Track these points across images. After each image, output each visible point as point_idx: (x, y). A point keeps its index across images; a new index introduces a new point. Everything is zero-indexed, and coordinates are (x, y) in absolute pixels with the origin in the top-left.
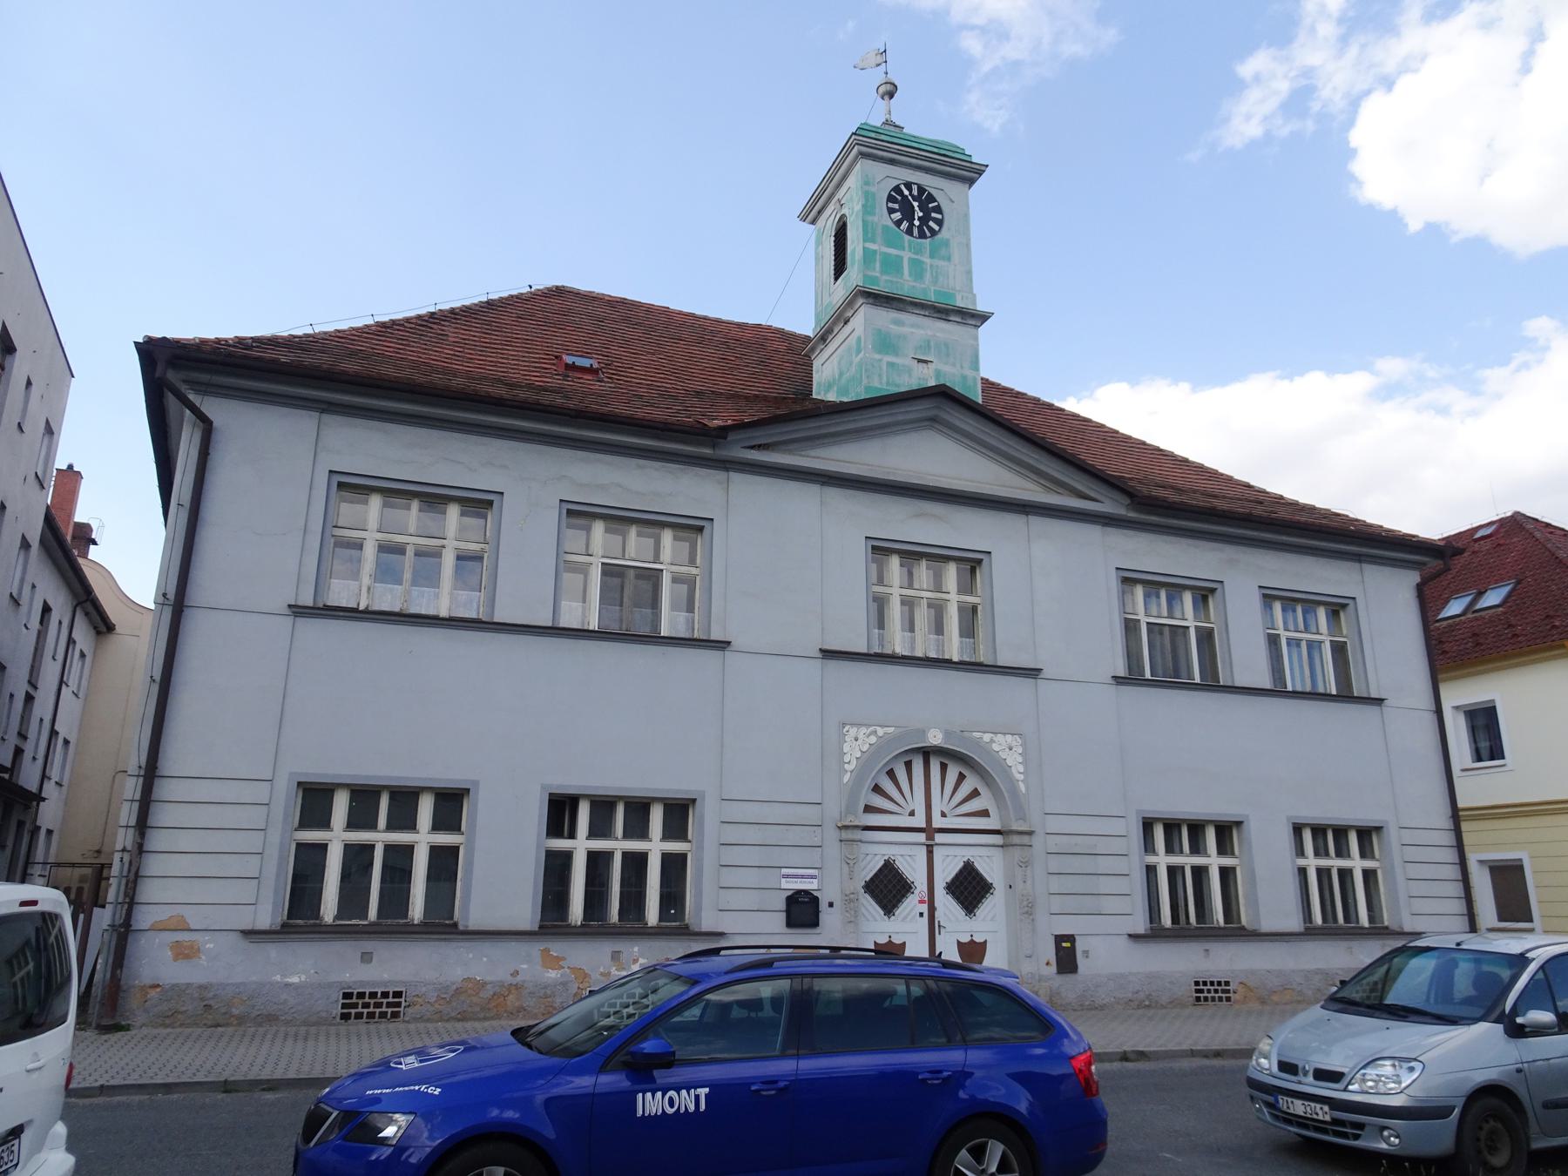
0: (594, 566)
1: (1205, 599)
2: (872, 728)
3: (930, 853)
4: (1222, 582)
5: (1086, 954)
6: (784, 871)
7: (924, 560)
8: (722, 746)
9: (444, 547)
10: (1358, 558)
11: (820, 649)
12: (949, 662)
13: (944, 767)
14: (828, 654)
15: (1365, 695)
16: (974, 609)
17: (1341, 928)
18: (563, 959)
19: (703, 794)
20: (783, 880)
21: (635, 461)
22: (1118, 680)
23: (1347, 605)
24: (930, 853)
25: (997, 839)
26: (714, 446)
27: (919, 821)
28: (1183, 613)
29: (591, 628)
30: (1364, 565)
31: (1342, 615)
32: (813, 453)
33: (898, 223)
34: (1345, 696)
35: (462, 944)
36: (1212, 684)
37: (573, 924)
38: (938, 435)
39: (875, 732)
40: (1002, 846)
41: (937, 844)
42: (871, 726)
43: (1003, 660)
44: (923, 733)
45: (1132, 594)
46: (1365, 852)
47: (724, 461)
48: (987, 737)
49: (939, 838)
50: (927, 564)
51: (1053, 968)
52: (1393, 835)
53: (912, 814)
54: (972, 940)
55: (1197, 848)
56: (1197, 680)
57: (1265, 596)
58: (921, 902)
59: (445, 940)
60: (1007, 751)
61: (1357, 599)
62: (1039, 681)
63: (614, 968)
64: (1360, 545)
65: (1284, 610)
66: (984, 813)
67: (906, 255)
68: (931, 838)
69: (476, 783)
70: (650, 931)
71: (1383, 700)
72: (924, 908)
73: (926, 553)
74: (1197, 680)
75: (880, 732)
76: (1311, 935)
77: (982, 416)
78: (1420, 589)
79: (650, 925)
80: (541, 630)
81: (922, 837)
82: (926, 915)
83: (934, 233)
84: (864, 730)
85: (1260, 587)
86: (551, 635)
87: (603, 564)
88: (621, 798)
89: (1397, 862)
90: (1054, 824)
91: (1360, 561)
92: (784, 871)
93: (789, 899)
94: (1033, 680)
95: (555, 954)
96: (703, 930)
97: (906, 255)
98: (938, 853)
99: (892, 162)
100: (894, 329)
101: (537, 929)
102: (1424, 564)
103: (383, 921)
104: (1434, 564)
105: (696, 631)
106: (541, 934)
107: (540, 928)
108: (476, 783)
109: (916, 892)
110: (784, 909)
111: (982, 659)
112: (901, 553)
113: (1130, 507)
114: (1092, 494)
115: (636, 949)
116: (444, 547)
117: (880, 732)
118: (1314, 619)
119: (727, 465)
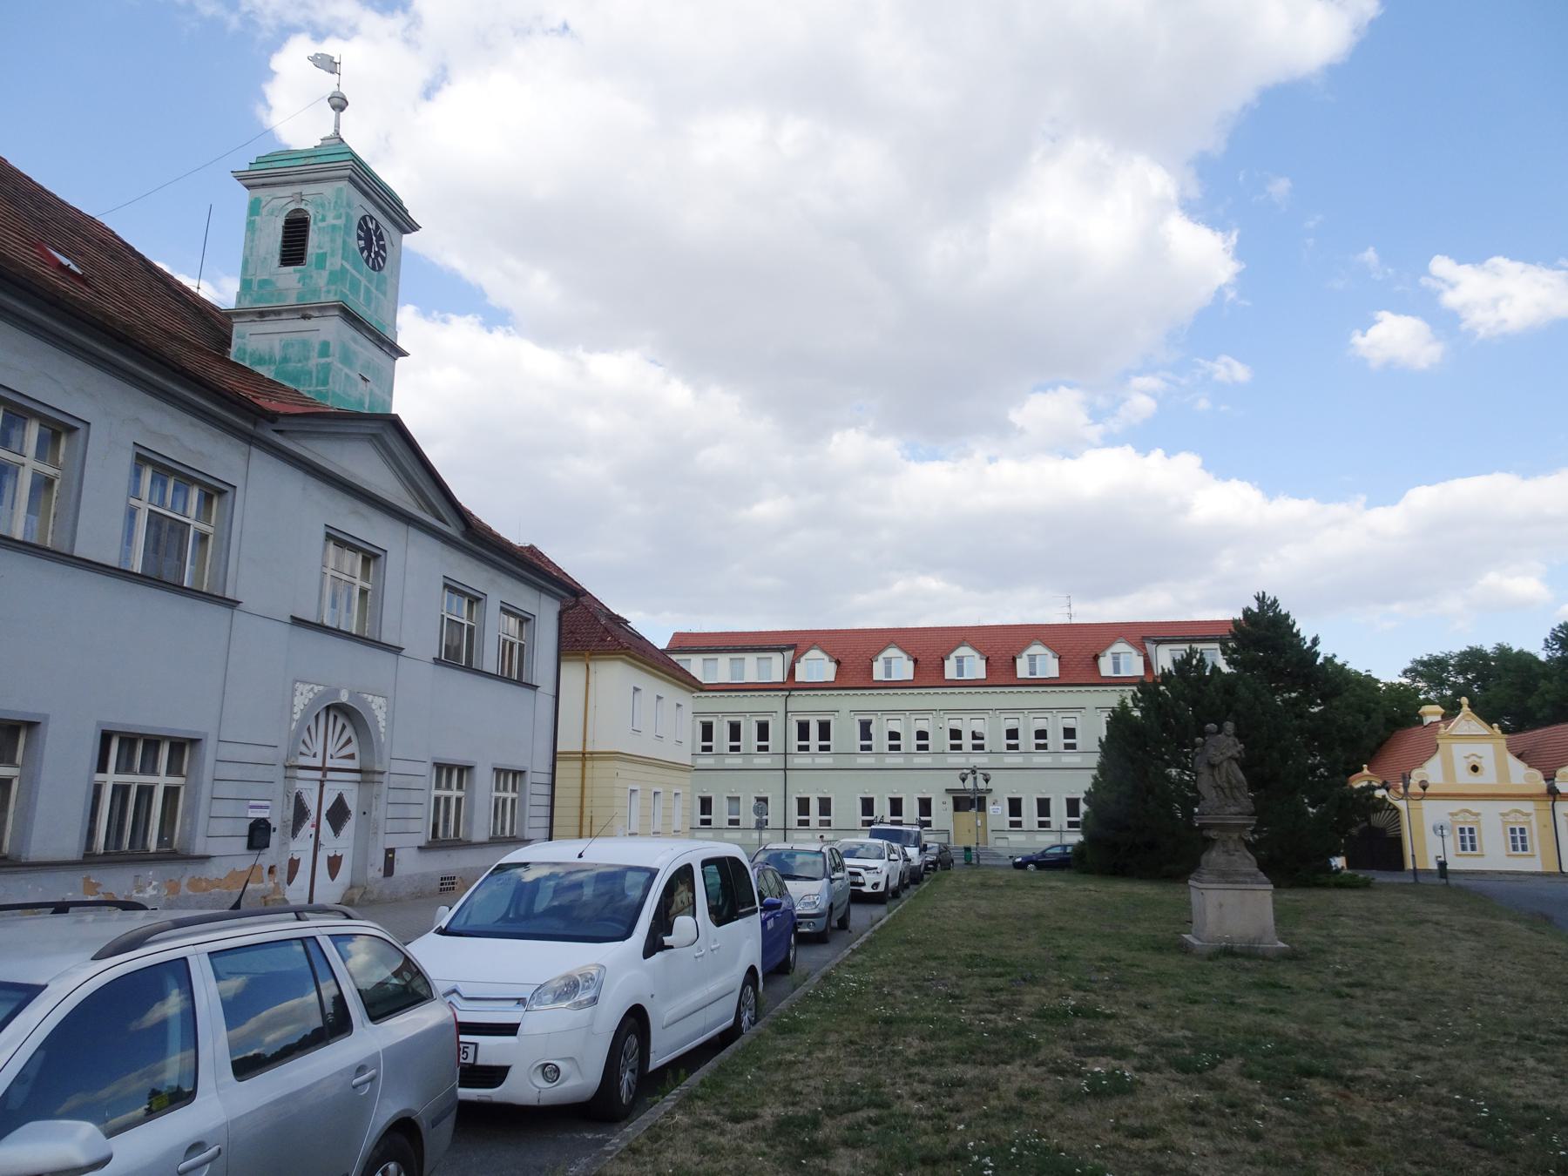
0: (142, 510)
1: (56, 437)
2: (311, 686)
3: (322, 786)
4: (386, 551)
5: (398, 860)
6: (252, 803)
7: (173, 478)
8: (224, 693)
9: (23, 465)
10: (541, 589)
11: (292, 616)
12: (350, 634)
13: (335, 717)
14: (297, 621)
15: (66, 550)
16: (49, 482)
17: (125, 853)
18: (99, 885)
19: (206, 734)
20: (250, 810)
21: (188, 418)
22: (437, 661)
23: (530, 619)
24: (322, 786)
25: (357, 777)
26: (255, 424)
27: (318, 762)
28: (21, 448)
29: (135, 571)
30: (542, 594)
31: (372, 562)
32: (303, 442)
33: (362, 250)
34: (520, 683)
35: (23, 876)
36: (469, 668)
37: (97, 853)
38: (373, 450)
39: (312, 689)
40: (359, 782)
41: (328, 780)
42: (311, 683)
43: (81, 551)
44: (337, 692)
45: (24, 429)
46: (172, 769)
47: (252, 437)
48: (370, 698)
49: (330, 775)
50: (448, 596)
51: (382, 873)
52: (209, 751)
53: (315, 756)
54: (335, 855)
55: (150, 767)
56: (464, 664)
57: (138, 456)
58: (313, 826)
59: (11, 873)
60: (377, 709)
61: (388, 553)
62: (400, 657)
63: (135, 891)
64: (547, 582)
65: (176, 489)
66: (352, 757)
67: (364, 282)
68: (324, 775)
69: (46, 717)
70: (151, 857)
71: (538, 687)
72: (313, 831)
73: (149, 458)
74: (464, 664)
75: (316, 689)
76: (90, 863)
77: (410, 447)
78: (561, 614)
79: (151, 851)
80: (83, 563)
81: (318, 775)
82: (313, 836)
83: (381, 268)
84: (308, 687)
85: (326, 525)
86: (316, 630)
87: (150, 511)
88: (165, 738)
89: (207, 778)
90: (397, 767)
91: (540, 591)
92: (252, 803)
93: (251, 825)
94: (228, 611)
95: (94, 881)
96: (31, 860)
97: (364, 282)
98: (327, 786)
99: (365, 194)
100: (353, 346)
101: (81, 859)
102: (563, 597)
103: (161, 850)
104: (571, 601)
105: (205, 585)
106: (85, 864)
107: (84, 857)
108: (46, 717)
109: (311, 818)
110: (247, 833)
111: (366, 634)
112: (44, 420)
113: (464, 535)
114: (447, 520)
115: (151, 873)
116: (23, 465)
117: (316, 689)
118: (183, 499)
119: (251, 440)
